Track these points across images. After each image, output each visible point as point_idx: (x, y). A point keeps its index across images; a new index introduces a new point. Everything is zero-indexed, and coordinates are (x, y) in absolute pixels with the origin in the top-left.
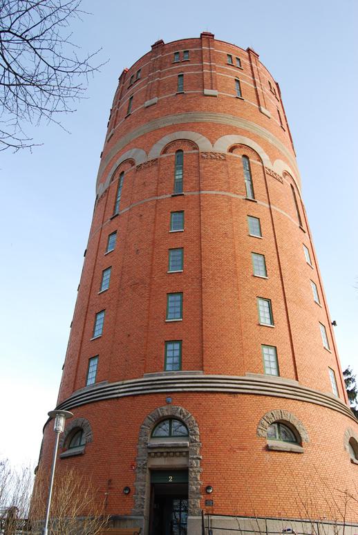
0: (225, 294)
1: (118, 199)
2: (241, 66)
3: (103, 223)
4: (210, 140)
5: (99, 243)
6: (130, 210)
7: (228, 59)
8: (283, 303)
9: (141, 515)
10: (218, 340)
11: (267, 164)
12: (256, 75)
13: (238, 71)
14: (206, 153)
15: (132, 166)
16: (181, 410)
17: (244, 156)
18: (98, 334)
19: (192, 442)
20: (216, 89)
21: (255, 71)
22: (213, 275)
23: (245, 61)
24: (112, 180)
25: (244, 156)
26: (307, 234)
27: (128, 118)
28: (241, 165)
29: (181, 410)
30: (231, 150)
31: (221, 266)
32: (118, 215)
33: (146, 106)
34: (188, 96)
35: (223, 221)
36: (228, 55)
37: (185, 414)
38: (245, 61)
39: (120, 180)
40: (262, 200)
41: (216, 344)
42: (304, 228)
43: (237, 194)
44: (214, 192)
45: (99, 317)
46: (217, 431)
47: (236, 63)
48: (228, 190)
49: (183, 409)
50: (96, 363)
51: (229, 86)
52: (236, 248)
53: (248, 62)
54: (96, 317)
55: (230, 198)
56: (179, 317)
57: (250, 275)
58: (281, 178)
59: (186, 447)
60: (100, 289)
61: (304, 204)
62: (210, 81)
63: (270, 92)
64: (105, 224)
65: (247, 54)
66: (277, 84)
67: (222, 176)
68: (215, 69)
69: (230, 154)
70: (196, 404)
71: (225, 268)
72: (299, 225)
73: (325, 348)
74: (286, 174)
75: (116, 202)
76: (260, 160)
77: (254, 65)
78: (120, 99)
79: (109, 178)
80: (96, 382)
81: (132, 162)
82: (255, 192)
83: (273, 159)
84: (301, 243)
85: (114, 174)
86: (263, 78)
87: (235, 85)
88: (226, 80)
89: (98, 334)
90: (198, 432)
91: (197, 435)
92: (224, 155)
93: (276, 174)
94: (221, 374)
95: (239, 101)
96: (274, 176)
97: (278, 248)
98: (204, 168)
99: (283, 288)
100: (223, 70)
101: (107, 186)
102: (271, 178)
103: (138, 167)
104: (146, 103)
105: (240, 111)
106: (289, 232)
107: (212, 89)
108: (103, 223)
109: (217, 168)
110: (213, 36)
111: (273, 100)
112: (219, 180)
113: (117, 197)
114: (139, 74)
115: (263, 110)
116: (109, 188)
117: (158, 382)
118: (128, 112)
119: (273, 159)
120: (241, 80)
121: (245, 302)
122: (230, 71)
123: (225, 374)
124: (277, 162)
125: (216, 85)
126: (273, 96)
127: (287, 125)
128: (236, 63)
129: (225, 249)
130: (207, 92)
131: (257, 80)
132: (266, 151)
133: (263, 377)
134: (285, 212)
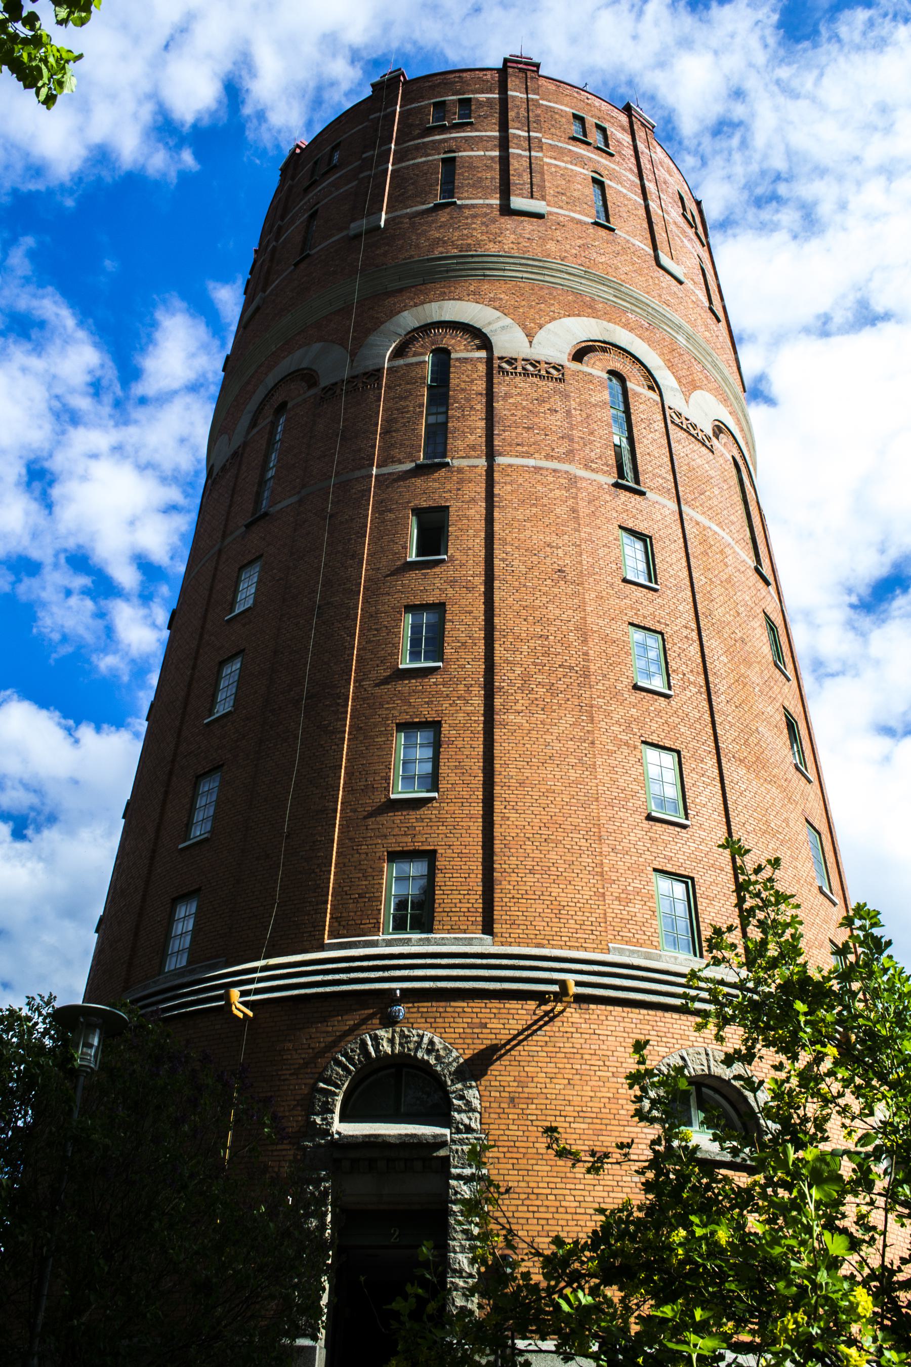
0: (555, 730)
1: (271, 473)
2: (607, 145)
3: (224, 536)
4: (524, 328)
5: (211, 589)
6: (300, 502)
7: (575, 129)
8: (711, 762)
9: (49, 71)
10: (537, 854)
11: (674, 399)
12: (647, 173)
13: (603, 160)
14: (511, 361)
15: (310, 387)
16: (431, 1042)
17: (613, 373)
18: (198, 832)
19: (459, 1131)
20: (543, 198)
21: (644, 161)
22: (526, 678)
23: (620, 136)
24: (254, 423)
25: (613, 373)
26: (772, 589)
27: (303, 266)
28: (606, 396)
29: (431, 1042)
30: (579, 355)
31: (546, 654)
32: (266, 514)
33: (352, 233)
34: (467, 212)
35: (554, 537)
36: (575, 117)
37: (442, 1053)
38: (620, 136)
39: (274, 425)
40: (660, 490)
41: (529, 863)
42: (766, 570)
43: (593, 470)
44: (531, 462)
45: (204, 787)
46: (530, 1099)
47: (595, 137)
48: (569, 456)
49: (436, 1040)
50: (193, 910)
51: (576, 194)
52: (589, 609)
53: (626, 139)
54: (196, 786)
55: (573, 480)
56: (429, 422)
57: (626, 681)
58: (709, 439)
59: (444, 1144)
60: (211, 713)
61: (765, 512)
62: (526, 177)
63: (681, 220)
64: (229, 539)
65: (624, 119)
66: (698, 203)
67: (555, 421)
68: (541, 149)
69: (575, 366)
70: (471, 1025)
71: (559, 660)
72: (752, 563)
73: (820, 888)
74: (719, 429)
75: (262, 482)
76: (654, 385)
77: (641, 146)
78: (282, 219)
79: (245, 420)
80: (189, 962)
81: (308, 377)
82: (640, 469)
83: (690, 386)
84: (759, 610)
85: (262, 405)
86: (665, 183)
87: (591, 191)
88: (568, 177)
89: (198, 832)
90: (476, 1103)
91: (474, 1110)
92: (558, 368)
93: (694, 427)
94: (543, 946)
95: (603, 233)
96: (690, 430)
97: (701, 617)
98: (507, 396)
99: (713, 722)
100: (560, 153)
101: (238, 439)
102: (682, 435)
103: (326, 389)
104: (352, 225)
105: (602, 259)
106: (729, 580)
107: (532, 197)
108: (224, 536)
109: (541, 401)
110: (538, 66)
111: (690, 240)
112: (546, 431)
113: (264, 468)
114: (336, 157)
115: (665, 260)
116: (245, 444)
117: (365, 964)
118: (303, 250)
119: (690, 386)
120: (607, 182)
121: (610, 753)
122: (582, 156)
123: (553, 947)
124: (697, 395)
125: (543, 188)
126: (691, 232)
127: (724, 308)
128: (595, 137)
129: (557, 612)
130: (517, 202)
131: (650, 186)
132: (671, 366)
133: (658, 958)
134: (719, 524)
